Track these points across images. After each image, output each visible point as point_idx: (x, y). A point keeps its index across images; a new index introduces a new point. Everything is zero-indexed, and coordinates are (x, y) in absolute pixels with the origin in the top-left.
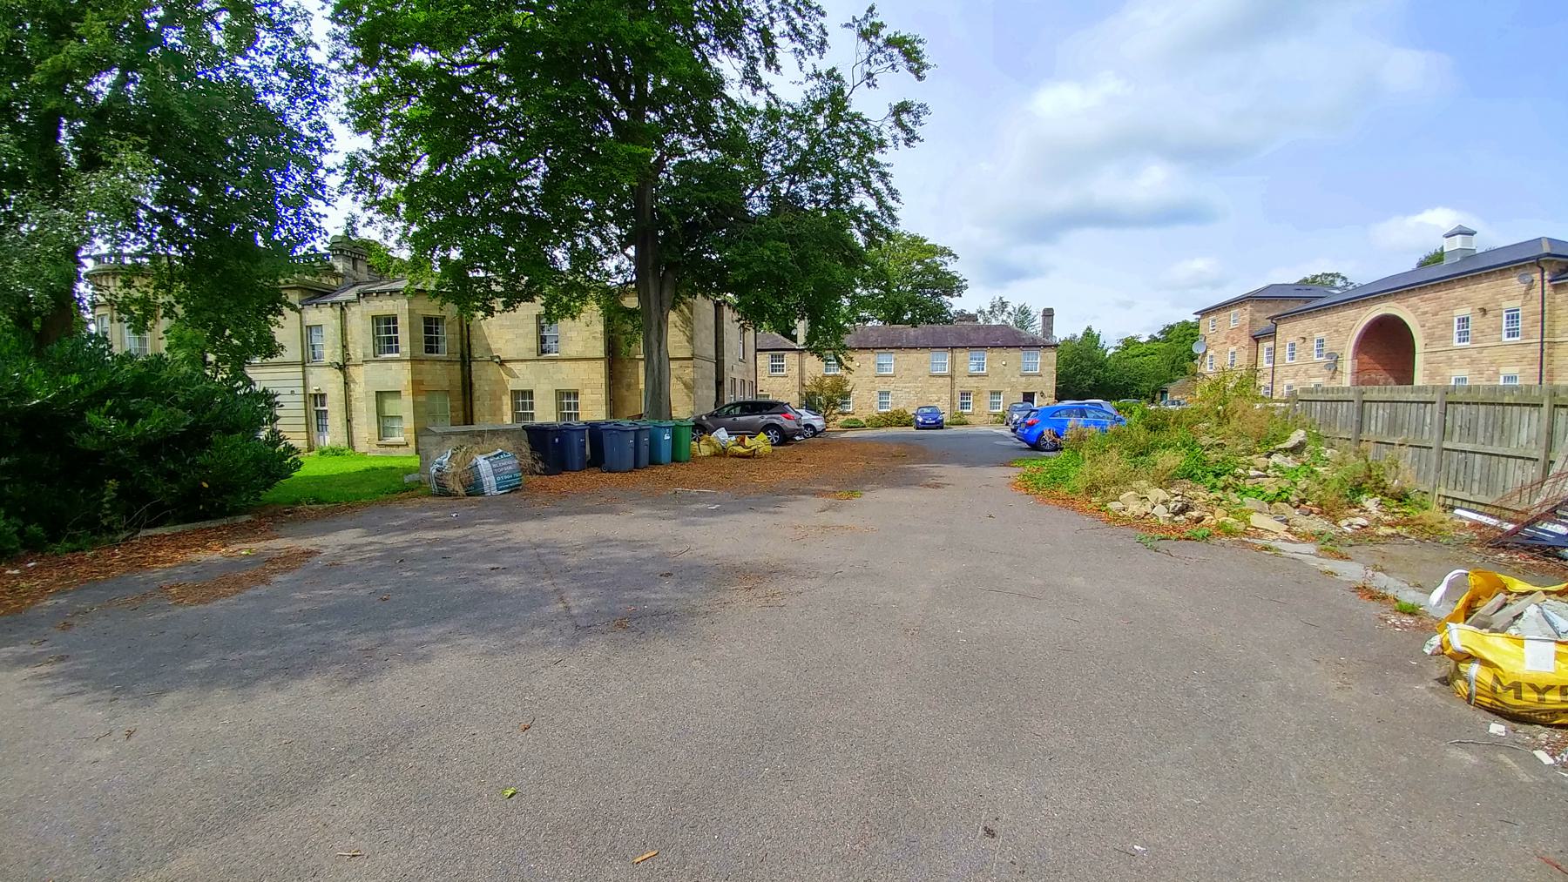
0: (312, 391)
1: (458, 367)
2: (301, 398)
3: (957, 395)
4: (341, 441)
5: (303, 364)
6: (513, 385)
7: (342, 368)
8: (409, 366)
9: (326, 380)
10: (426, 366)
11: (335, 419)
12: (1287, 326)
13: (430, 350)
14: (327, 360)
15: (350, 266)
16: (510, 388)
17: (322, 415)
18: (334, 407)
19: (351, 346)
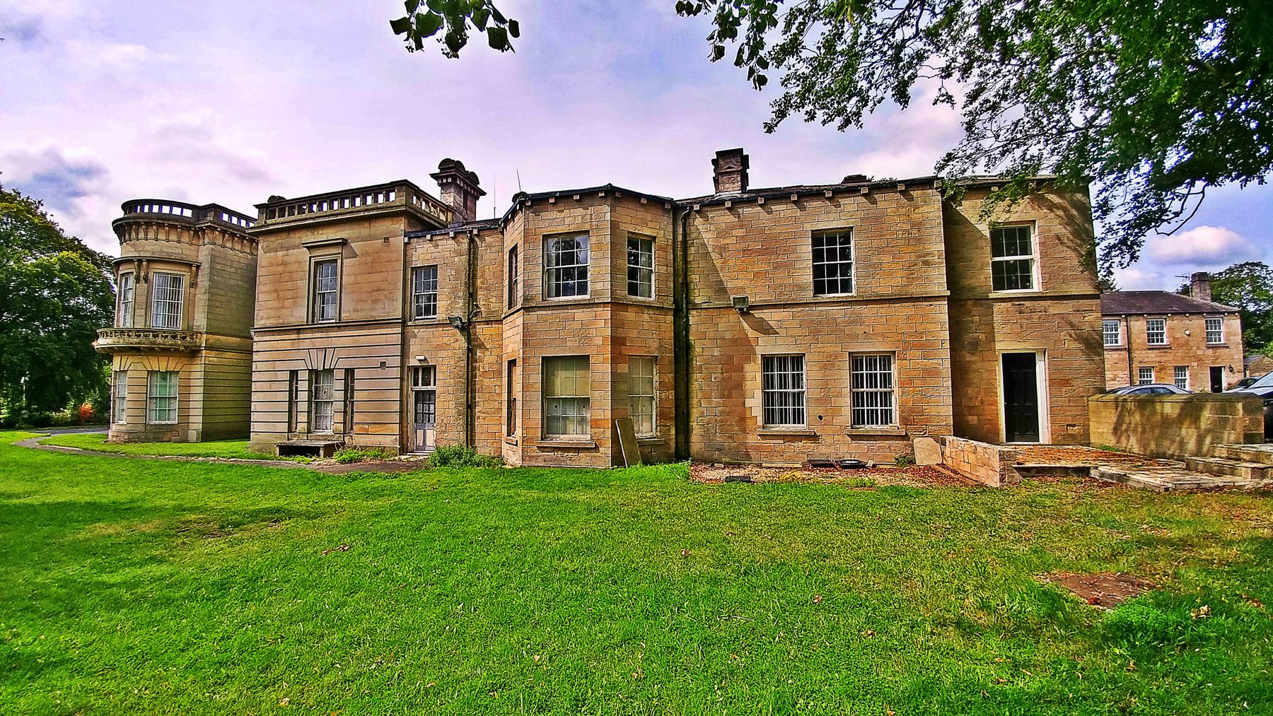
0: (413, 362)
1: (670, 318)
2: (396, 373)
3: (1136, 372)
4: (455, 438)
5: (404, 324)
6: (766, 346)
7: (466, 328)
8: (607, 313)
9: (438, 346)
10: (630, 315)
11: (447, 404)
12: (569, 374)
13: (633, 290)
14: (441, 315)
15: (460, 200)
16: (760, 351)
17: (425, 398)
18: (446, 389)
19: (481, 295)
